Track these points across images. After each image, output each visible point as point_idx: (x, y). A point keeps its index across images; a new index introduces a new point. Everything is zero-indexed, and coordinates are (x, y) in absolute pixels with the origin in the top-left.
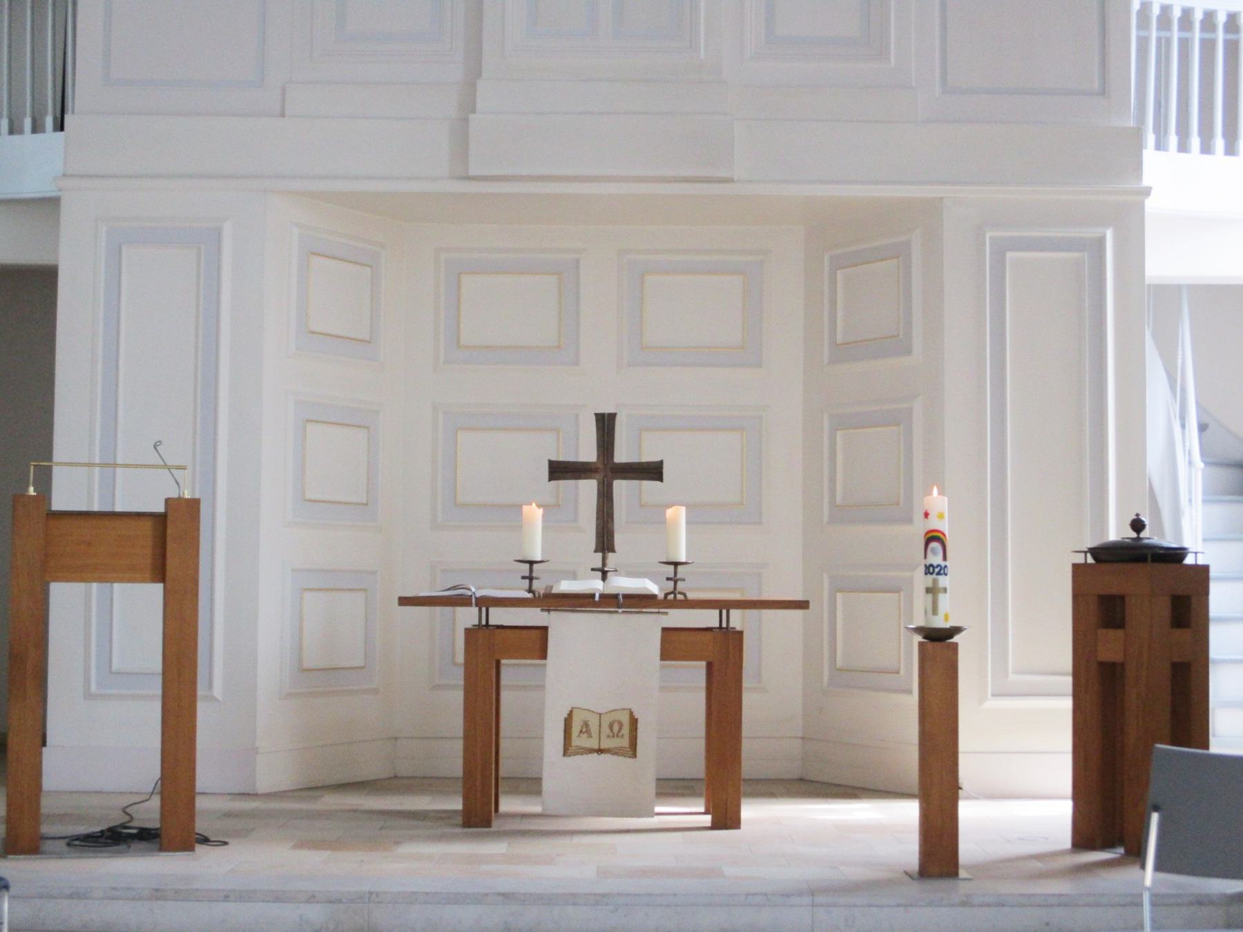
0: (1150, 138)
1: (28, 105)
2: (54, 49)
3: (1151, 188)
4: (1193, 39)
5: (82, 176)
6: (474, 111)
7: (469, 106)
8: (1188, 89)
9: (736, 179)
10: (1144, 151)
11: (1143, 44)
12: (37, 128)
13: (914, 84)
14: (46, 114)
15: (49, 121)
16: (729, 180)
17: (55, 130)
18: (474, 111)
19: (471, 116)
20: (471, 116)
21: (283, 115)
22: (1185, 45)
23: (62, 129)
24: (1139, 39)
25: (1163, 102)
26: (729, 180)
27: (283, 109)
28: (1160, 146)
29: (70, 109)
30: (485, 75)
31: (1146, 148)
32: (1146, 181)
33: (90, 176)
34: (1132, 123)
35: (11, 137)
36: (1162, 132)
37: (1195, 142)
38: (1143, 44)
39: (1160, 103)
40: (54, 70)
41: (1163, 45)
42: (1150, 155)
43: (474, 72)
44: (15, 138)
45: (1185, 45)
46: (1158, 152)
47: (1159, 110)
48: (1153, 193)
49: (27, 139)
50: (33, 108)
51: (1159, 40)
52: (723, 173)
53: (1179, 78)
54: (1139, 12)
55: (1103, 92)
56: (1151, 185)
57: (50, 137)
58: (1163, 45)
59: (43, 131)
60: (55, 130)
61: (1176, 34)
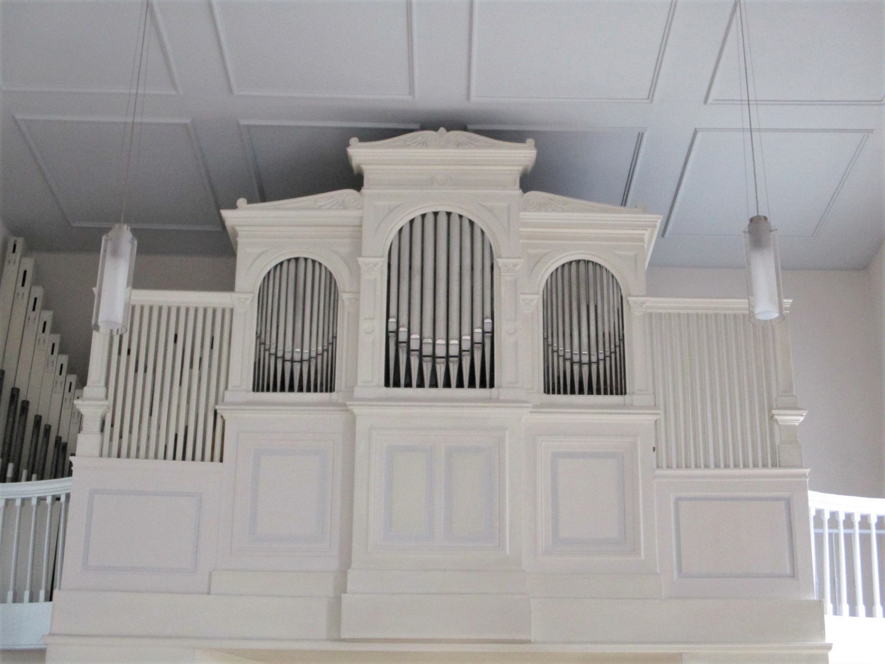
0: (829, 606)
1: (28, 582)
2: (50, 538)
3: (832, 644)
4: (854, 534)
5: (84, 636)
6: (345, 592)
7: (341, 587)
8: (853, 568)
9: (533, 640)
10: (825, 616)
11: (819, 538)
12: (33, 599)
13: (658, 571)
14: (25, 589)
15: (42, 594)
16: (528, 642)
17: (46, 600)
18: (345, 592)
19: (343, 595)
20: (343, 595)
21: (209, 593)
22: (849, 539)
23: (51, 600)
24: (817, 535)
25: (836, 579)
26: (528, 642)
27: (209, 588)
28: (836, 612)
29: (58, 586)
30: (354, 565)
31: (826, 614)
32: (828, 640)
33: (89, 636)
34: (815, 597)
35: (31, 604)
36: (837, 603)
37: (861, 608)
38: (819, 538)
39: (834, 580)
40: (49, 550)
41: (834, 539)
42: (829, 618)
43: (346, 564)
44: (34, 604)
45: (849, 539)
46: (835, 616)
47: (834, 586)
48: (833, 646)
49: (26, 607)
50: (15, 584)
51: (830, 535)
52: (519, 637)
53: (847, 564)
54: (815, 518)
55: (793, 575)
56: (832, 643)
57: (42, 606)
58: (834, 539)
59: (37, 600)
60: (46, 600)
61: (842, 531)
